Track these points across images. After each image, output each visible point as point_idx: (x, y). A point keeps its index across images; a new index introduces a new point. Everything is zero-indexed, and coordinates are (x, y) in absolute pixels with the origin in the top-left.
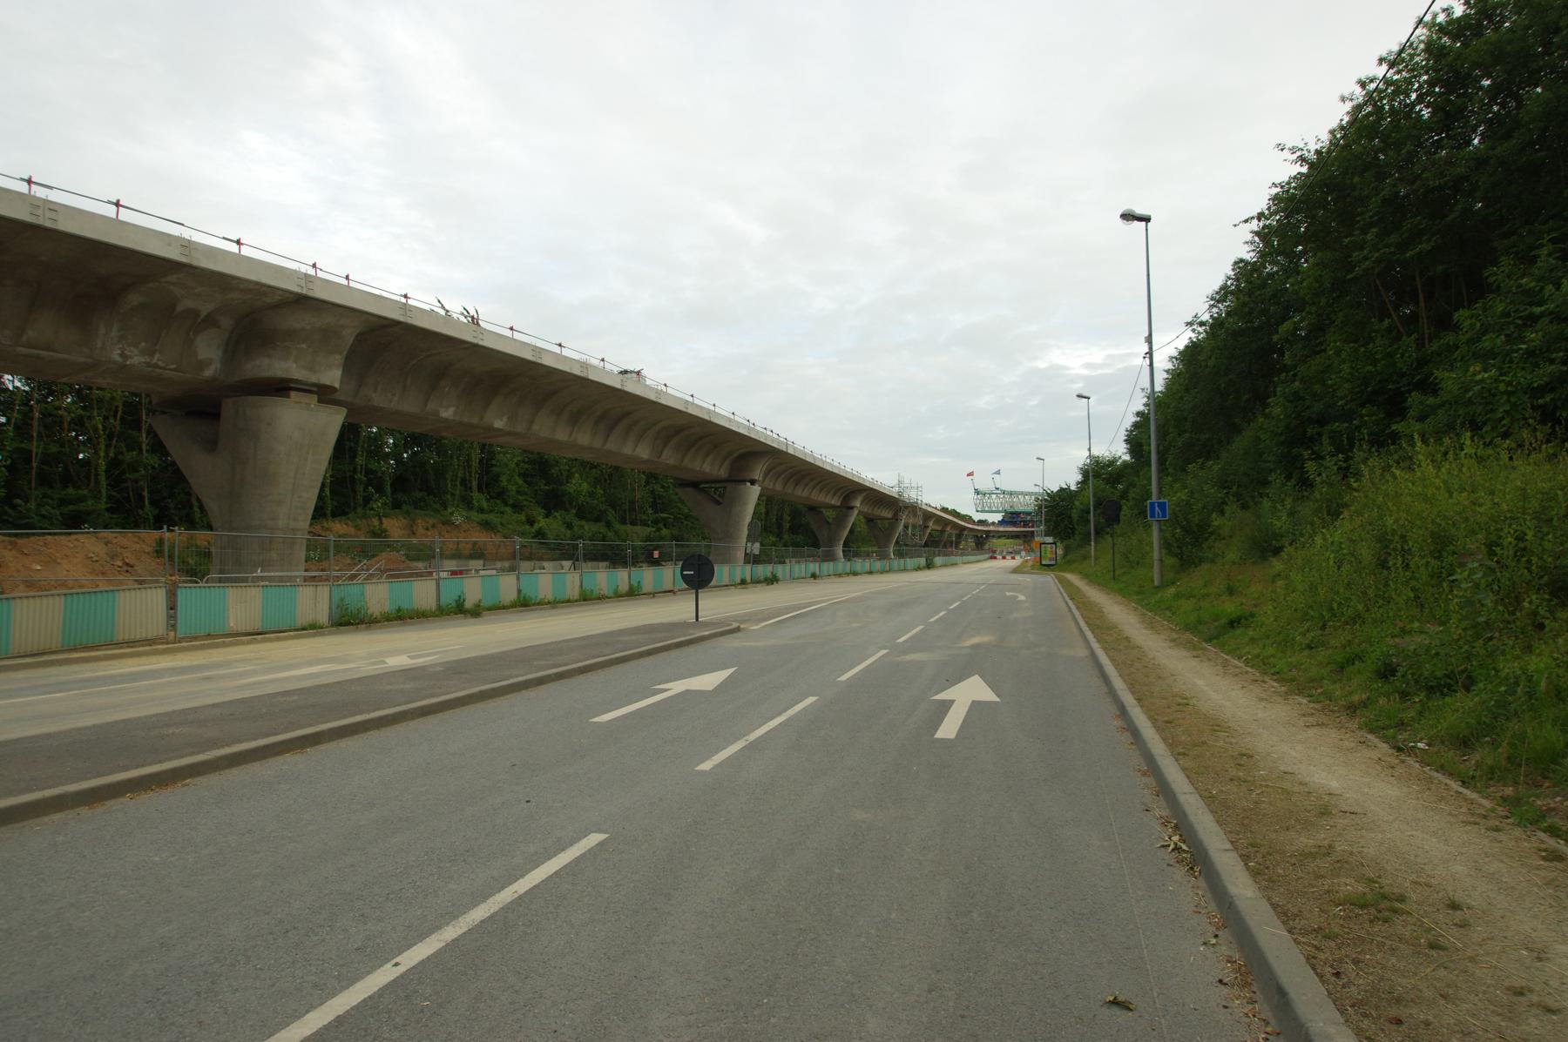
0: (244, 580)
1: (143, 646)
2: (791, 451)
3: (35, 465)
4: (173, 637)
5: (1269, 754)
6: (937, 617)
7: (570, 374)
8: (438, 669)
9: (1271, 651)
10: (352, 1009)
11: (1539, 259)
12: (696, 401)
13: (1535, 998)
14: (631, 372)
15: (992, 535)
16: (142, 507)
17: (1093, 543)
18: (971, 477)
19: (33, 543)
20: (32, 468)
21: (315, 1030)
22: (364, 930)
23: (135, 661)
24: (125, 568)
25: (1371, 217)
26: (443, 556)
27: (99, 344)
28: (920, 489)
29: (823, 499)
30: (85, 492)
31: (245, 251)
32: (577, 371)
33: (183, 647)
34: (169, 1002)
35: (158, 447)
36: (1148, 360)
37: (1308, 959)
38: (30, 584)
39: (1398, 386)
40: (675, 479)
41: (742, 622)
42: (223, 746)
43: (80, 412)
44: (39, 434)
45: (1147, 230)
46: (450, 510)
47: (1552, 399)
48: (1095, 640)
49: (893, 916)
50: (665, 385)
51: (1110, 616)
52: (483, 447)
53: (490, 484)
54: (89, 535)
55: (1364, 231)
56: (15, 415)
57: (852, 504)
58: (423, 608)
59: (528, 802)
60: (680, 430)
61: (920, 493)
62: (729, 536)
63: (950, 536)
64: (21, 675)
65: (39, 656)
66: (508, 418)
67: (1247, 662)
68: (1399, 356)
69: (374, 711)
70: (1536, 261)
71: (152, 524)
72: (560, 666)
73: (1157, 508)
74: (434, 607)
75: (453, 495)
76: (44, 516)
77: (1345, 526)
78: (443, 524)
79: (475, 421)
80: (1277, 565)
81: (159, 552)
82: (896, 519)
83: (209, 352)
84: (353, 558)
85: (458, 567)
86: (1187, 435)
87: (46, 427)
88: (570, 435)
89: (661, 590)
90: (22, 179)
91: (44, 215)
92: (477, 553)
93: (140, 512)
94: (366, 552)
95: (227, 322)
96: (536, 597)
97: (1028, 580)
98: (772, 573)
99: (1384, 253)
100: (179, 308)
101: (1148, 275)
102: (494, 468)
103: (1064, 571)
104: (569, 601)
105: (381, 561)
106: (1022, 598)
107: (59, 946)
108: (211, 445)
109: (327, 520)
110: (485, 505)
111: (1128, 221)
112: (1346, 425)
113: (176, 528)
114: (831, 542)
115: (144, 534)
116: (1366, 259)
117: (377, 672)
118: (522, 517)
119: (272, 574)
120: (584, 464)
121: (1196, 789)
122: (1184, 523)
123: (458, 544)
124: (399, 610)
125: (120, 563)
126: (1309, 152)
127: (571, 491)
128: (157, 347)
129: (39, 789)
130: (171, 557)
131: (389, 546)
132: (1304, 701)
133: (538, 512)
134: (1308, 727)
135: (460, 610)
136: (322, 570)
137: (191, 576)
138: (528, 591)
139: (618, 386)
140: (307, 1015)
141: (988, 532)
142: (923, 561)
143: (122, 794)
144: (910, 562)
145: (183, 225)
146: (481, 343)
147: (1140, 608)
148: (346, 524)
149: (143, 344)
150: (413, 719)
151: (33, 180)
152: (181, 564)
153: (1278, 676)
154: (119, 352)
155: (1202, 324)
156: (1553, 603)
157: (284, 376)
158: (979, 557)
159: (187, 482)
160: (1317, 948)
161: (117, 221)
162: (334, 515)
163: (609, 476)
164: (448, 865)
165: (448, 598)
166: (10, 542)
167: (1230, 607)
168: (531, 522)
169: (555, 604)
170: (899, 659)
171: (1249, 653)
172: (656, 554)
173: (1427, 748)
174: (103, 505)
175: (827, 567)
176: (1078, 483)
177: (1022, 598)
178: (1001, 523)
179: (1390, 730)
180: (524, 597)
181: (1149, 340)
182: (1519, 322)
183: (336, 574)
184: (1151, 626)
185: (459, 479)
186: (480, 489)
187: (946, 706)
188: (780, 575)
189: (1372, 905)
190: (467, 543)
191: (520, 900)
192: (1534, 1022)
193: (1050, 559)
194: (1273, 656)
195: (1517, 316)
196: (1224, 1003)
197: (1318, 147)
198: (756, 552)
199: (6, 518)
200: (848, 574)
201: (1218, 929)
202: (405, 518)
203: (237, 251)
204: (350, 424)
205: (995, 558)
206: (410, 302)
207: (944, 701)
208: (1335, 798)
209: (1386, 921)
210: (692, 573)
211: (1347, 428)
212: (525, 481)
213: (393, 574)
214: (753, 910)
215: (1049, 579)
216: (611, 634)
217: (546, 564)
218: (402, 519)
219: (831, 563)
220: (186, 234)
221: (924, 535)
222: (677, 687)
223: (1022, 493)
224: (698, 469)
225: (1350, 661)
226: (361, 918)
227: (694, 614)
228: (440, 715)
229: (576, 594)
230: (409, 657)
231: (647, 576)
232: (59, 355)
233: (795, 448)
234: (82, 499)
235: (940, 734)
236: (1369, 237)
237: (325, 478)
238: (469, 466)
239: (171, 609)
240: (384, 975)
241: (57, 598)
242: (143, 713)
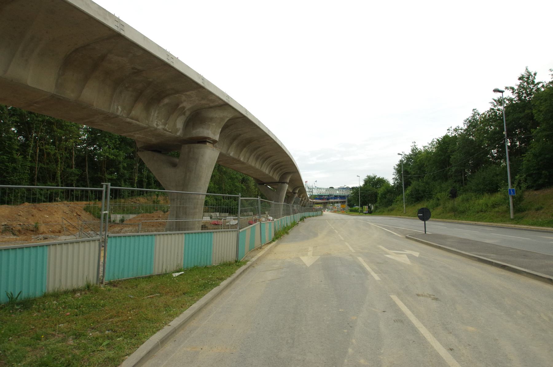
71: (31, 201)
148: (144, 198)
176: (363, 185)
193: (366, 211)
210: (422, 215)
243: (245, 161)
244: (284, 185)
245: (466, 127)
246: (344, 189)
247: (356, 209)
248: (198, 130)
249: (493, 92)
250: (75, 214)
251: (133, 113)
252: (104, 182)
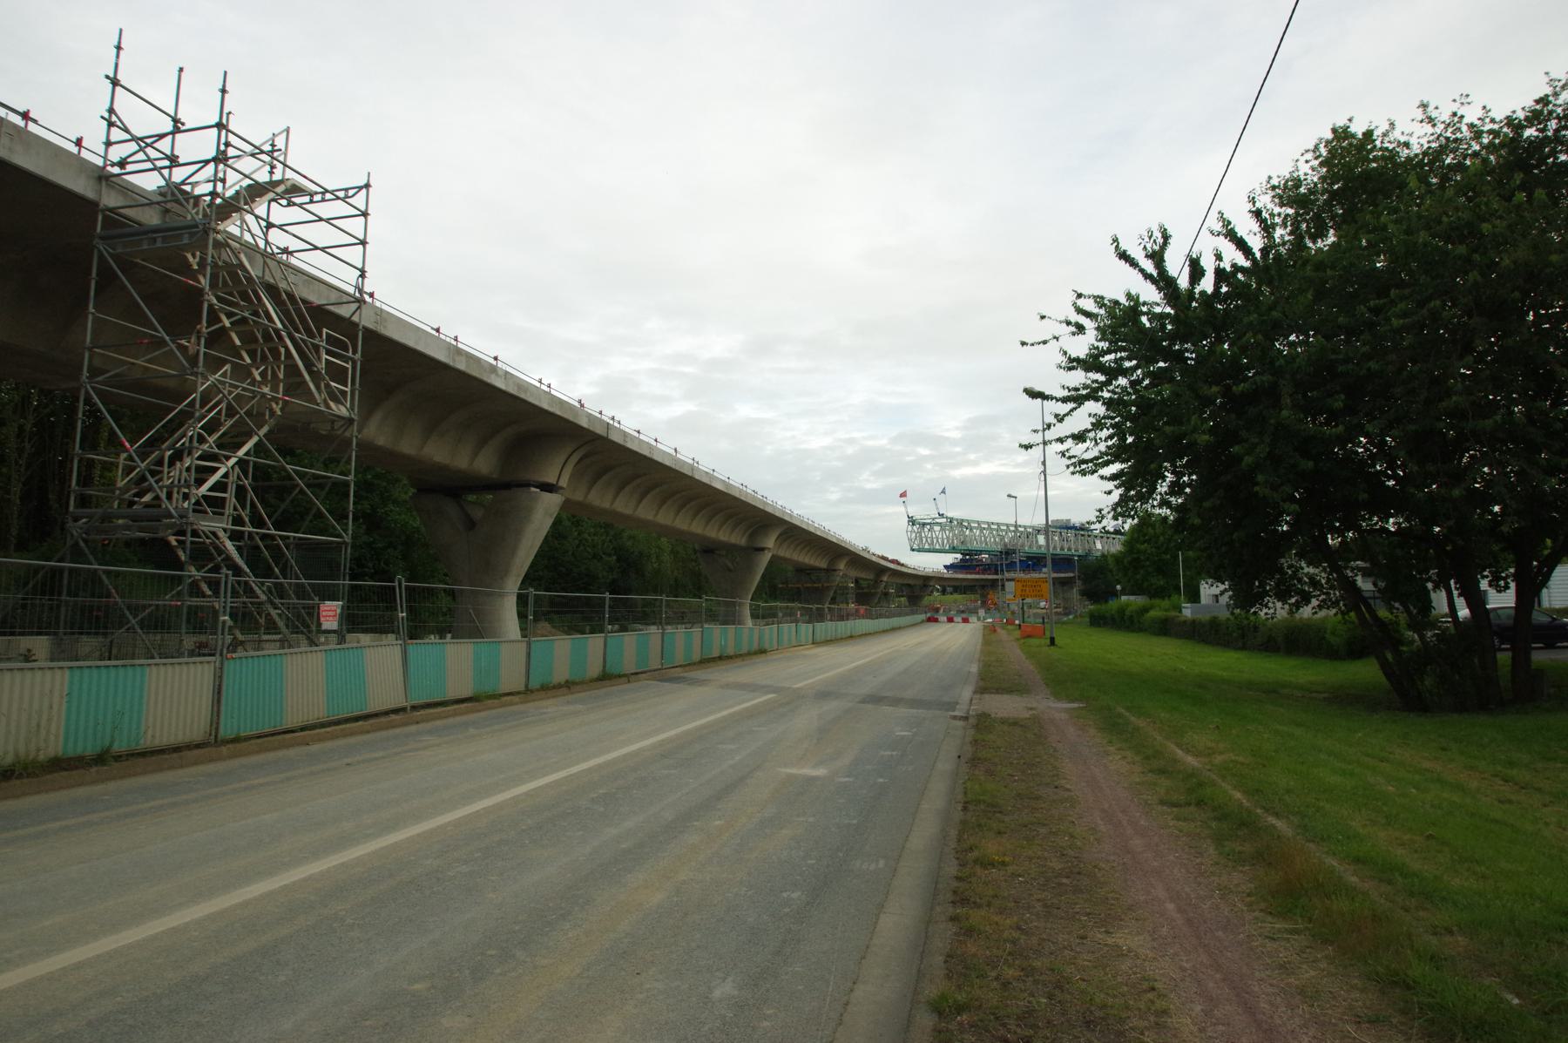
18: (904, 499)
57: (837, 568)
181: (1044, 463)
205: (936, 620)
246: (1071, 528)
247: (1128, 613)
252: (1110, 560)
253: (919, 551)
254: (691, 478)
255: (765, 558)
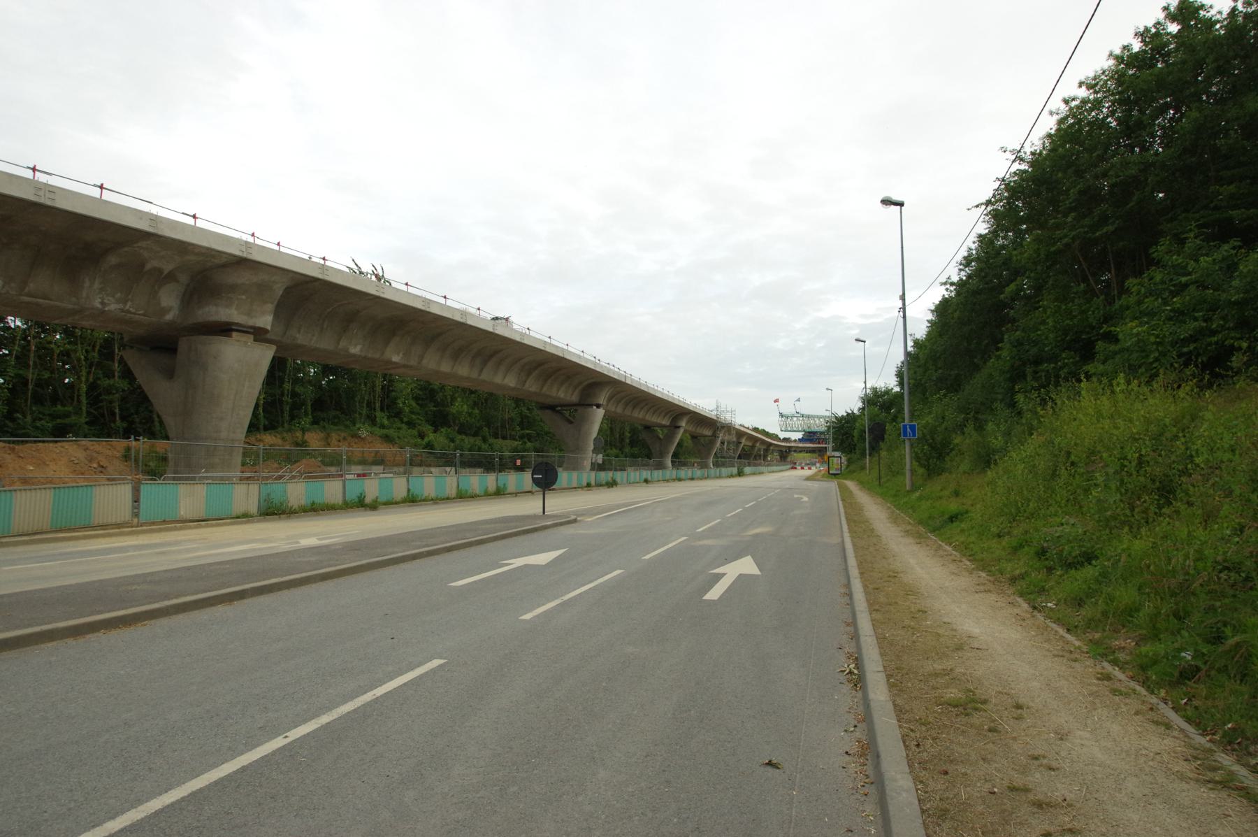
0: (193, 479)
1: (113, 529)
2: (628, 382)
3: (30, 387)
4: (137, 522)
5: (940, 611)
6: (734, 513)
7: (453, 320)
8: (337, 547)
9: (972, 539)
10: (253, 762)
11: (1187, 241)
12: (553, 342)
13: (1045, 761)
14: (501, 318)
15: (793, 449)
16: (114, 421)
17: (867, 457)
18: (777, 403)
19: (27, 449)
20: (28, 390)
21: (227, 774)
22: (266, 717)
23: (107, 540)
24: (100, 469)
25: (1070, 203)
26: (349, 462)
27: (84, 295)
28: (733, 413)
29: (655, 421)
30: (70, 409)
31: (200, 224)
32: (458, 318)
33: (145, 530)
34: (130, 757)
35: (127, 374)
36: (901, 314)
37: (903, 736)
38: (25, 481)
39: (1090, 336)
40: (537, 403)
41: (578, 516)
42: (172, 599)
43: (68, 347)
44: (34, 362)
45: (901, 212)
46: (358, 426)
47: (1195, 348)
48: (847, 531)
49: (636, 712)
50: (528, 329)
51: (867, 514)
52: (385, 376)
53: (390, 405)
54: (71, 443)
55: (1066, 216)
56: (16, 348)
58: (332, 502)
59: (392, 638)
60: (540, 364)
61: (733, 416)
62: (579, 449)
63: (759, 450)
64: (20, 549)
65: (34, 535)
66: (403, 354)
67: (955, 548)
68: (1090, 313)
69: (286, 576)
70: (1185, 242)
71: (121, 435)
72: (432, 546)
73: (908, 429)
74: (341, 502)
75: (360, 414)
76: (37, 428)
77: (1036, 440)
78: (352, 437)
79: (377, 356)
80: (990, 474)
81: (126, 457)
82: (714, 436)
83: (170, 300)
84: (279, 464)
85: (363, 470)
86: (940, 371)
87: (39, 357)
88: (453, 367)
89: (521, 491)
90: (28, 168)
91: (45, 195)
92: (379, 461)
93: (113, 425)
94: (290, 459)
95: (184, 278)
96: (422, 495)
97: (816, 486)
98: (612, 478)
99: (1079, 232)
100: (148, 267)
101: (902, 248)
102: (393, 393)
103: (846, 479)
104: (448, 499)
105: (301, 466)
106: (805, 499)
107: (54, 724)
108: (170, 374)
109: (260, 433)
110: (386, 422)
111: (886, 205)
112: (1053, 365)
113: (141, 438)
114: (662, 454)
115: (115, 443)
116: (1066, 236)
117: (292, 549)
118: (415, 432)
119: (215, 475)
120: (464, 390)
121: (876, 633)
122: (931, 441)
123: (363, 453)
124: (313, 503)
125: (95, 465)
126: (1026, 153)
127: (454, 411)
128: (130, 297)
129: (38, 625)
130: (136, 461)
131: (308, 454)
132: (984, 575)
133: (427, 429)
134: (977, 592)
135: (361, 504)
136: (255, 472)
137: (152, 476)
138: (416, 490)
139: (491, 330)
140: (223, 766)
141: (790, 447)
142: (735, 470)
143: (98, 630)
144: (724, 471)
145: (151, 203)
146: (382, 295)
147: (892, 507)
148: (275, 436)
149: (119, 294)
150: (315, 582)
151: (37, 168)
152: (144, 467)
153: (972, 557)
154: (100, 300)
155: (952, 284)
156: (1161, 502)
157: (227, 320)
158: (784, 467)
159: (149, 401)
160: (912, 730)
161: (100, 201)
162: (266, 429)
163: (485, 401)
164: (328, 678)
165: (352, 495)
166: (10, 448)
167: (953, 506)
168: (422, 436)
169: (437, 501)
170: (693, 544)
171: (957, 540)
172: (519, 462)
173: (1054, 607)
174: (83, 419)
175: (658, 474)
176: (860, 409)
177: (805, 499)
178: (800, 440)
179: (1033, 594)
180: (412, 495)
181: (903, 298)
182: (1172, 288)
183: (265, 475)
184: (895, 520)
185: (366, 402)
186: (382, 409)
187: (719, 577)
188: (618, 480)
189: (961, 706)
190: (370, 452)
191: (376, 700)
192: (1038, 775)
193: (836, 469)
194: (973, 543)
195: (1171, 284)
196: (844, 765)
197: (1032, 150)
198: (600, 461)
199: (6, 429)
200: (674, 480)
201: (858, 722)
202: (322, 432)
203: (193, 224)
204: (279, 358)
205: (796, 468)
206: (328, 263)
207: (718, 574)
208: (971, 639)
209: (967, 715)
211: (1054, 368)
212: (418, 404)
213: (309, 476)
214: (538, 707)
215: (833, 485)
216: (476, 523)
217: (433, 470)
218: (320, 433)
219: (706, 470)
220: (154, 210)
221: (737, 450)
222: (518, 562)
223: (817, 417)
224: (554, 395)
225: (1021, 546)
226: (264, 710)
227: (542, 510)
228: (335, 580)
229: (454, 493)
230: (317, 539)
231: (512, 479)
232: (52, 303)
233: (632, 380)
234: (67, 415)
235: (708, 597)
236: (1069, 219)
237: (258, 399)
238: (374, 391)
239: (136, 502)
240: (278, 743)
241: (48, 491)
242: (113, 576)
243: (413, 362)
244: (590, 409)
245: (963, 275)
248: (207, 309)
249: (880, 204)
250: (95, 465)
251: (31, 286)
253: (785, 431)
254: (625, 384)
255: (742, 445)
